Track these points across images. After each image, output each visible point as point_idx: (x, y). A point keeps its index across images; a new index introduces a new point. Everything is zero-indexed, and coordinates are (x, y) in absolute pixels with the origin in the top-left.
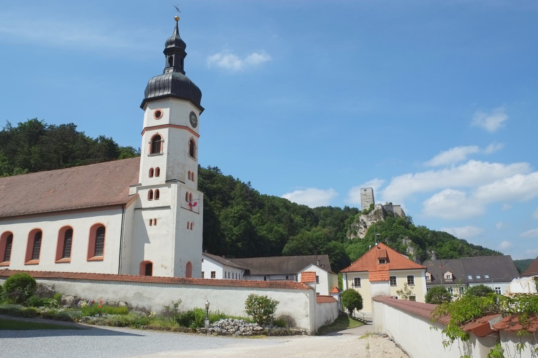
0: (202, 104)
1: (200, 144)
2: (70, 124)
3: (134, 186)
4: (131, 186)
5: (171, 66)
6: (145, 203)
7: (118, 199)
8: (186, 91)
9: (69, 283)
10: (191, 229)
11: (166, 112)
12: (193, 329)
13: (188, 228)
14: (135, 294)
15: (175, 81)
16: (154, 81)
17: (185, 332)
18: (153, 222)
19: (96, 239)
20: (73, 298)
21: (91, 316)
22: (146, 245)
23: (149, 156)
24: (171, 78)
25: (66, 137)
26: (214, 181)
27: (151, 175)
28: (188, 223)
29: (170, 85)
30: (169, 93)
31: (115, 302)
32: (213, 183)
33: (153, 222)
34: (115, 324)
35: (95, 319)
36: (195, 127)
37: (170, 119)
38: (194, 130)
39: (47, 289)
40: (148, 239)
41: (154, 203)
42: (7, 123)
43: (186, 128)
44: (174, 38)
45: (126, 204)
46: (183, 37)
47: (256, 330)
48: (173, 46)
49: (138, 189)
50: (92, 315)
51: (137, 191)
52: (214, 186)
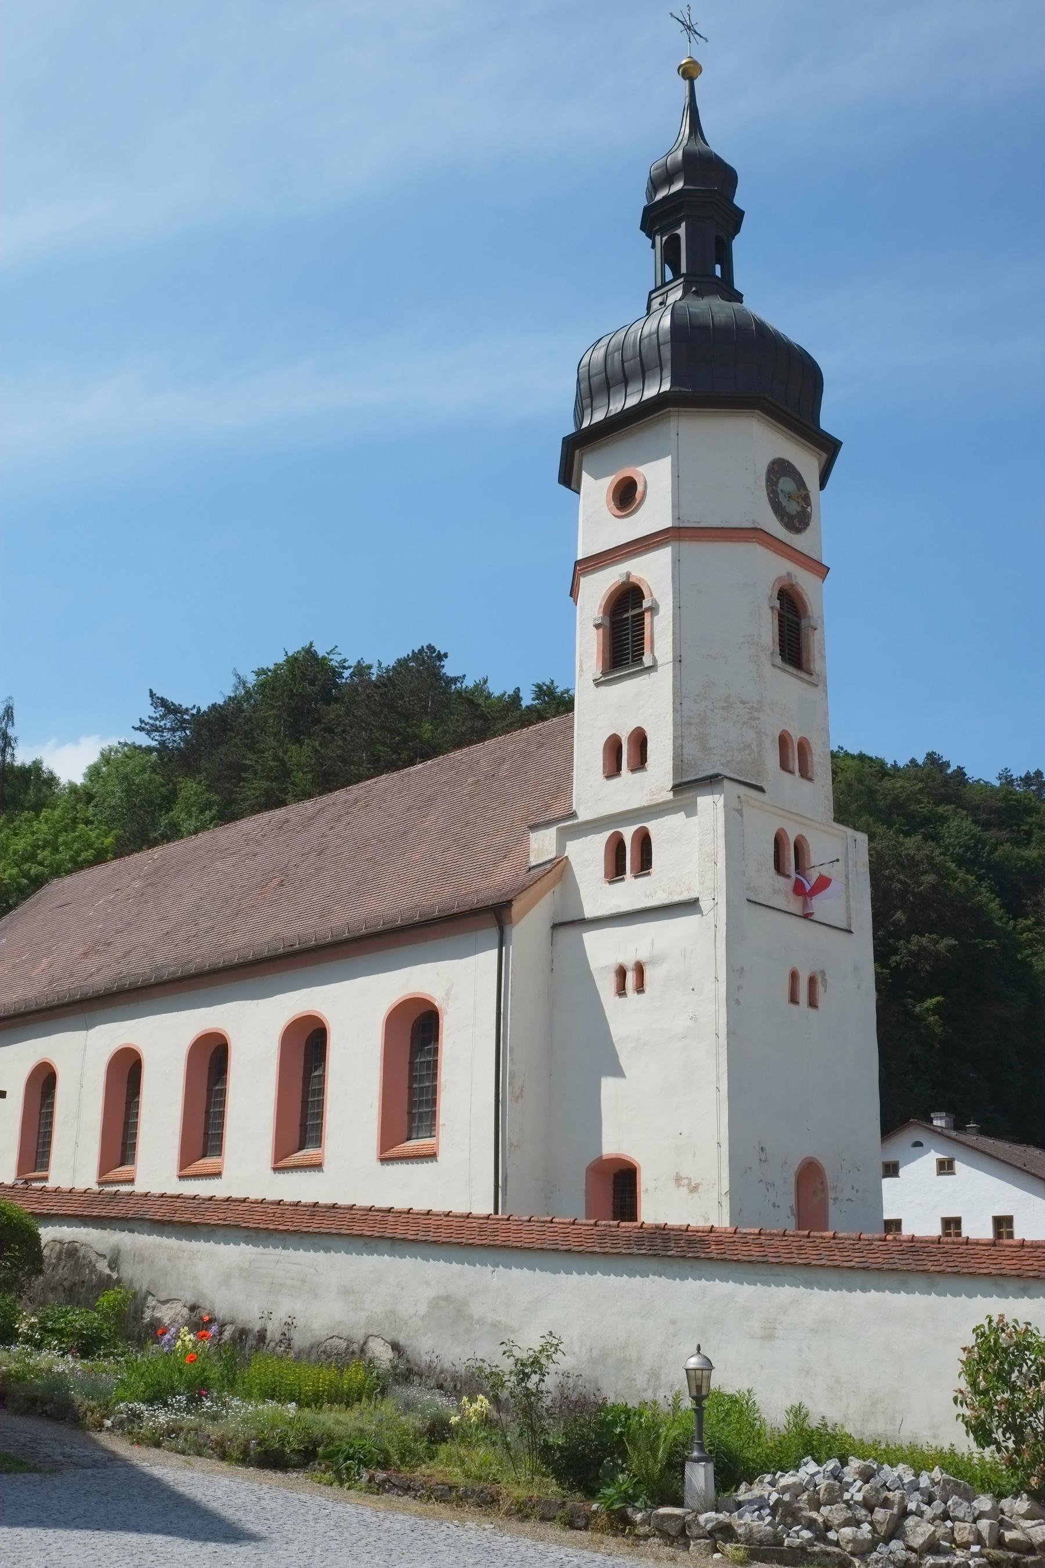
0: (829, 421)
1: (830, 607)
2: (421, 651)
3: (548, 824)
4: (535, 827)
5: (677, 274)
6: (597, 895)
7: (482, 888)
8: (736, 370)
9: (172, 1242)
10: (813, 1004)
11: (656, 476)
12: (610, 1512)
13: (794, 999)
14: (435, 1304)
15: (684, 331)
16: (599, 354)
17: (571, 1524)
18: (631, 978)
19: (411, 1063)
20: (185, 1312)
21: (150, 1402)
22: (608, 1085)
23: (598, 683)
24: (667, 322)
25: (402, 698)
26: (1029, 834)
27: (613, 769)
28: (794, 976)
29: (666, 353)
30: (666, 387)
31: (350, 1341)
32: (1026, 841)
33: (631, 978)
34: (245, 1452)
35: (163, 1418)
36: (798, 531)
37: (676, 506)
38: (798, 541)
39: (93, 1269)
40: (615, 1056)
41: (632, 892)
42: (234, 680)
43: (754, 534)
44: (679, 154)
45: (509, 904)
46: (719, 142)
47: (1015, 1546)
48: (678, 186)
49: (567, 835)
50: (157, 1397)
51: (561, 846)
52: (1031, 853)
